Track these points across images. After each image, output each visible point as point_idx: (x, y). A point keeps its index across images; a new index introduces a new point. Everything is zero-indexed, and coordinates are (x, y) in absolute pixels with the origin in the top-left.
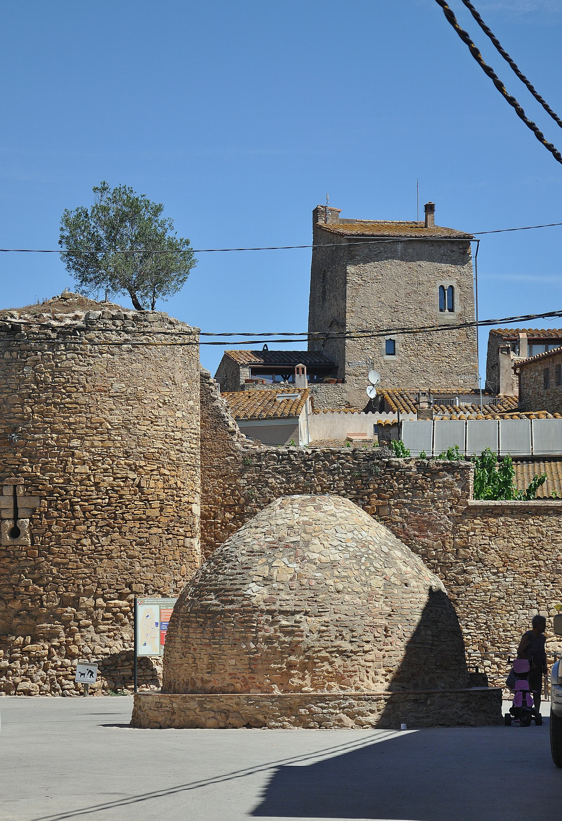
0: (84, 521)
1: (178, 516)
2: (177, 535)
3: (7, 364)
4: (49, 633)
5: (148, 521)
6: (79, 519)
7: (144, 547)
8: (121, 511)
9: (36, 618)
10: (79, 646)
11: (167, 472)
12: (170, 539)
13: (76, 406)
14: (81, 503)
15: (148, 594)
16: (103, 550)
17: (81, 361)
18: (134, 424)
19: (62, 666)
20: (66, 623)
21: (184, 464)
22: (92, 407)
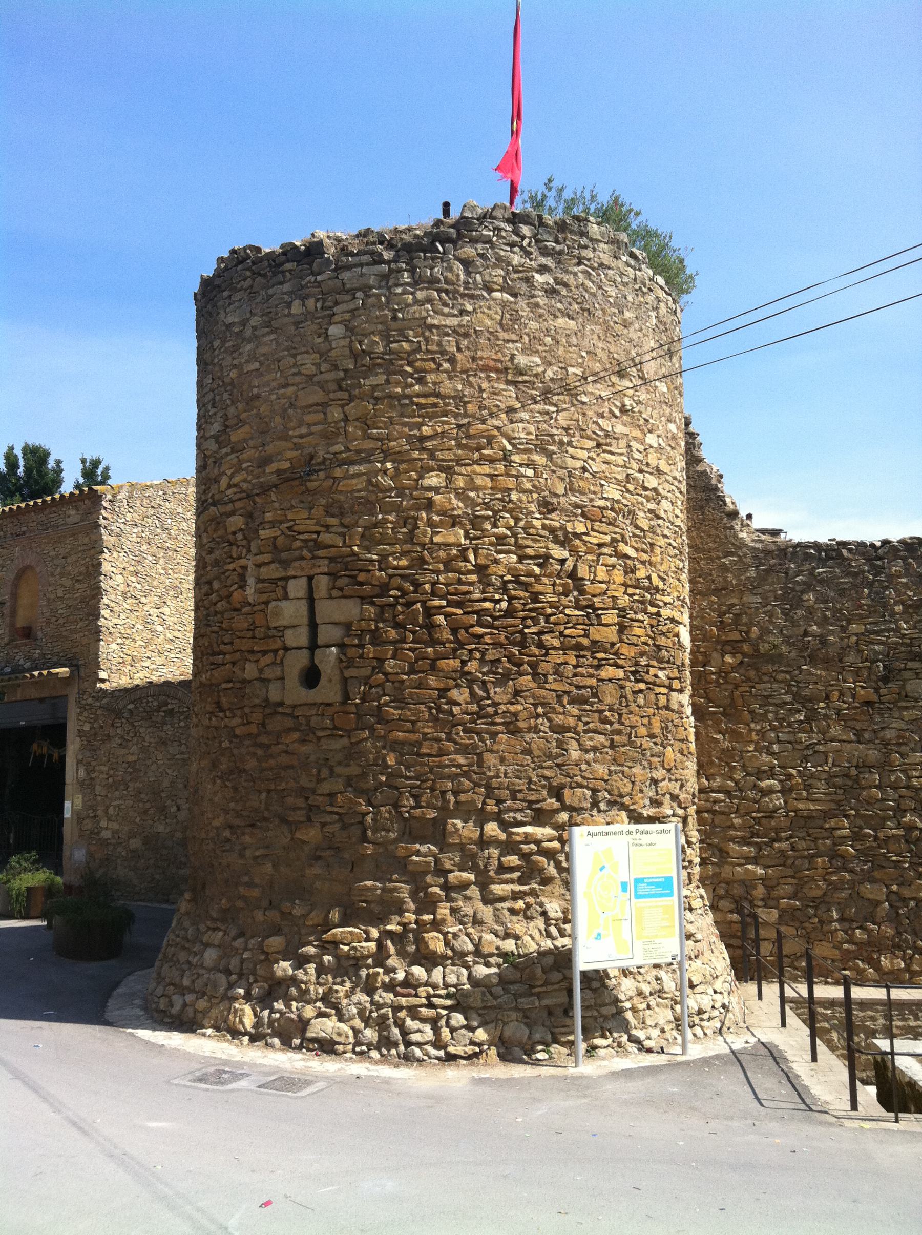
0: (455, 650)
1: (654, 645)
2: (654, 684)
3: (297, 324)
4: (381, 901)
5: (593, 653)
6: (444, 644)
7: (588, 708)
8: (534, 630)
9: (355, 866)
10: (445, 934)
11: (631, 553)
12: (641, 691)
13: (435, 400)
14: (448, 609)
15: (599, 811)
16: (496, 713)
17: (446, 305)
18: (561, 443)
19: (406, 983)
20: (416, 879)
21: (662, 542)
22: (469, 402)
